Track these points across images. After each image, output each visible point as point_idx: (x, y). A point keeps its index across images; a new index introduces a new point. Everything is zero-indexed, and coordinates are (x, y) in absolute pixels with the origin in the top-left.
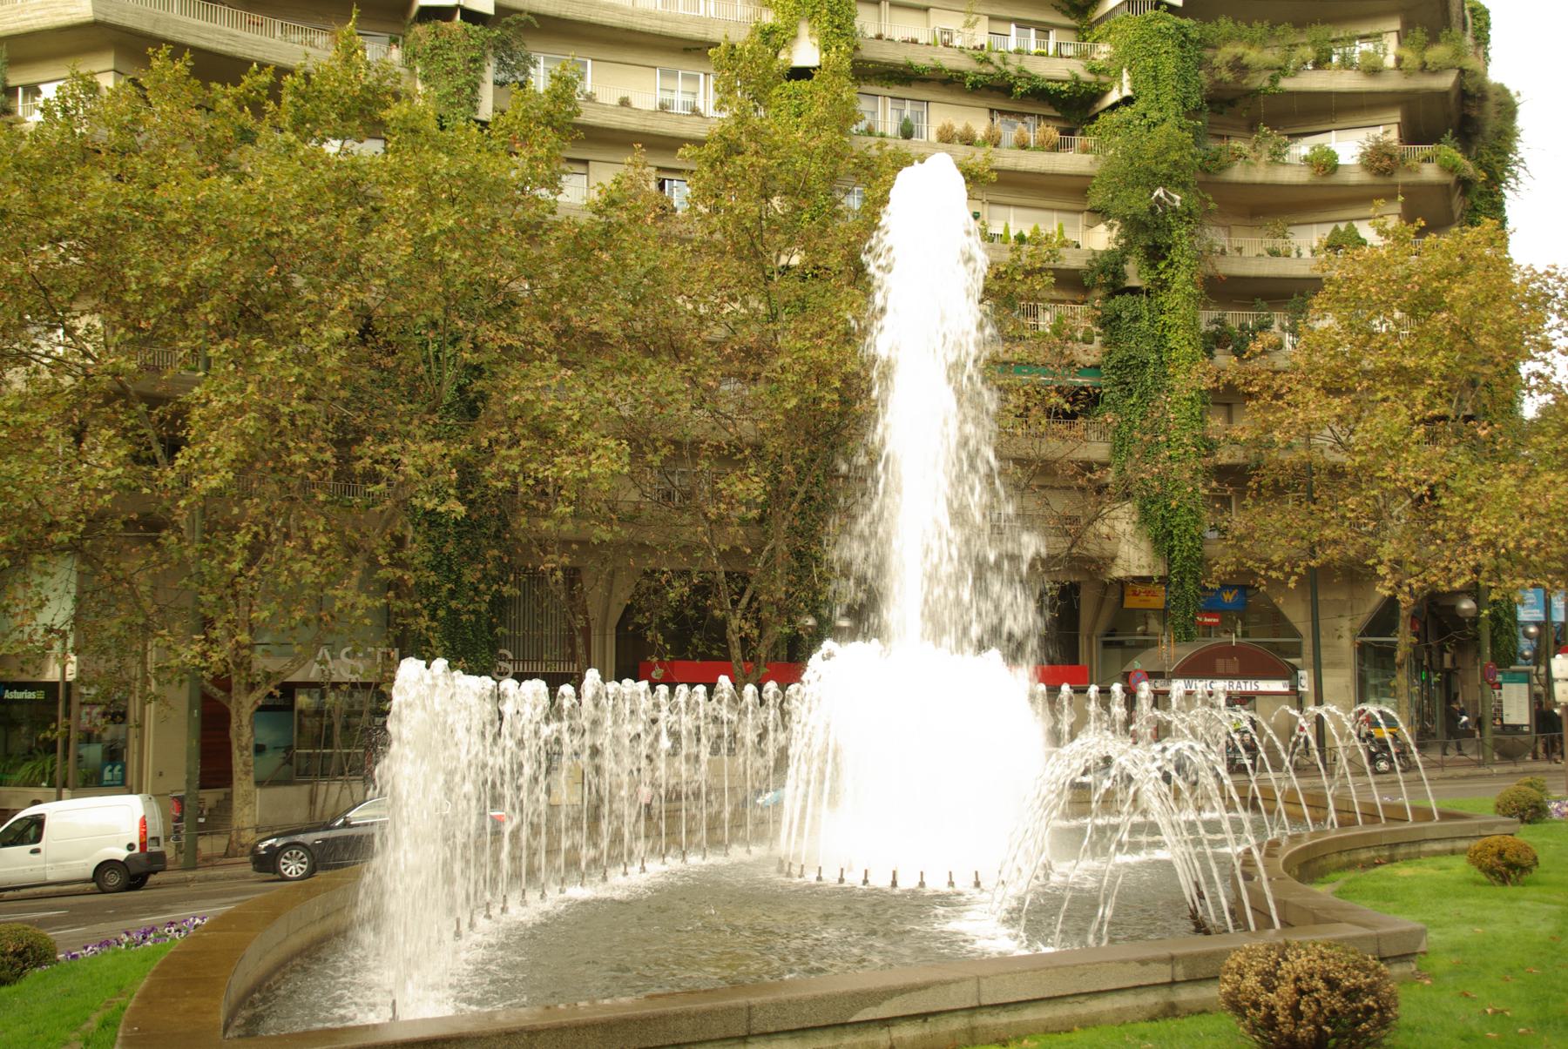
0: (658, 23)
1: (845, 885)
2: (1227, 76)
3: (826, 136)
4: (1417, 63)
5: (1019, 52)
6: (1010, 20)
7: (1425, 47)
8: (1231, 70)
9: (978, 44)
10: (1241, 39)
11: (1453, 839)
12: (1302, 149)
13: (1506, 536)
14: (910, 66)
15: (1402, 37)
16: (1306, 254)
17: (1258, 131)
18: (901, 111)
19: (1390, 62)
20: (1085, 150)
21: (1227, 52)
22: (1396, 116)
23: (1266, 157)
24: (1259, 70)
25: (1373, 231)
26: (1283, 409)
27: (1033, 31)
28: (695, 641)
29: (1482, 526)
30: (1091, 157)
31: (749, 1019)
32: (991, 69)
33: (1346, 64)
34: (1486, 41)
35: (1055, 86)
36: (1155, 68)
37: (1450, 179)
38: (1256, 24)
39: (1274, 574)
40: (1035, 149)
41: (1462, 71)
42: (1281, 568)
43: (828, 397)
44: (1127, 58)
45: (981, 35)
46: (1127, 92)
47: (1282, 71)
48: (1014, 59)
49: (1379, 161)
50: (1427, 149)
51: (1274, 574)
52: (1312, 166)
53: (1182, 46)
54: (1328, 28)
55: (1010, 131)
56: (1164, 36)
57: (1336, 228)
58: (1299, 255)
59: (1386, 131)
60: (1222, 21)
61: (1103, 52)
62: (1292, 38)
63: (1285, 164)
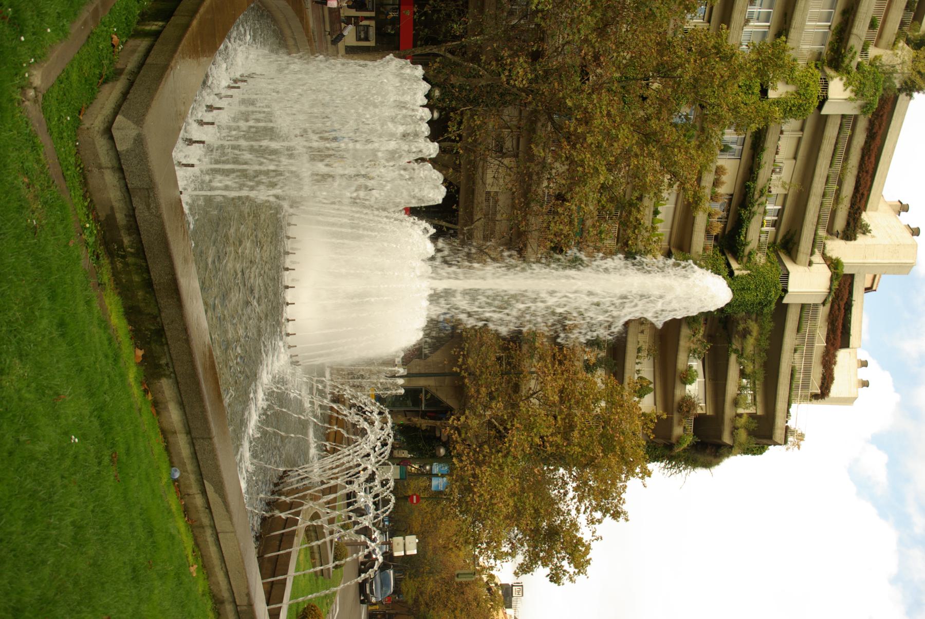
0: (803, 6)
1: (285, 240)
2: (741, 327)
3: (729, 115)
4: (739, 425)
5: (765, 212)
6: (783, 206)
7: (747, 429)
8: (744, 329)
9: (772, 189)
10: (761, 334)
11: (320, 553)
12: (696, 365)
13: (481, 487)
14: (763, 150)
15: (752, 416)
16: (638, 367)
17: (708, 342)
18: (736, 143)
19: (740, 411)
20: (705, 249)
21: (754, 328)
22: (710, 412)
23: (693, 346)
24: (742, 344)
25: (647, 404)
26: (553, 366)
27: (776, 218)
28: (426, 30)
29: (486, 473)
30: (701, 252)
31: (203, 438)
32: (756, 196)
33: (741, 388)
34: (746, 453)
35: (744, 233)
36: (749, 289)
37: (674, 440)
38: (768, 342)
39: (460, 360)
40: (708, 221)
41: (731, 447)
42: (464, 363)
43: (572, 125)
44: (756, 273)
45: (777, 190)
46: (736, 273)
47: (740, 355)
48: (761, 210)
49: (687, 404)
50: (691, 428)
51: (460, 360)
52: (686, 371)
53: (760, 303)
54: (762, 380)
55: (718, 208)
56: (767, 294)
57: (651, 383)
58: (637, 363)
59: (703, 407)
60: (772, 324)
61: (760, 259)
62: (758, 361)
63: (688, 356)
